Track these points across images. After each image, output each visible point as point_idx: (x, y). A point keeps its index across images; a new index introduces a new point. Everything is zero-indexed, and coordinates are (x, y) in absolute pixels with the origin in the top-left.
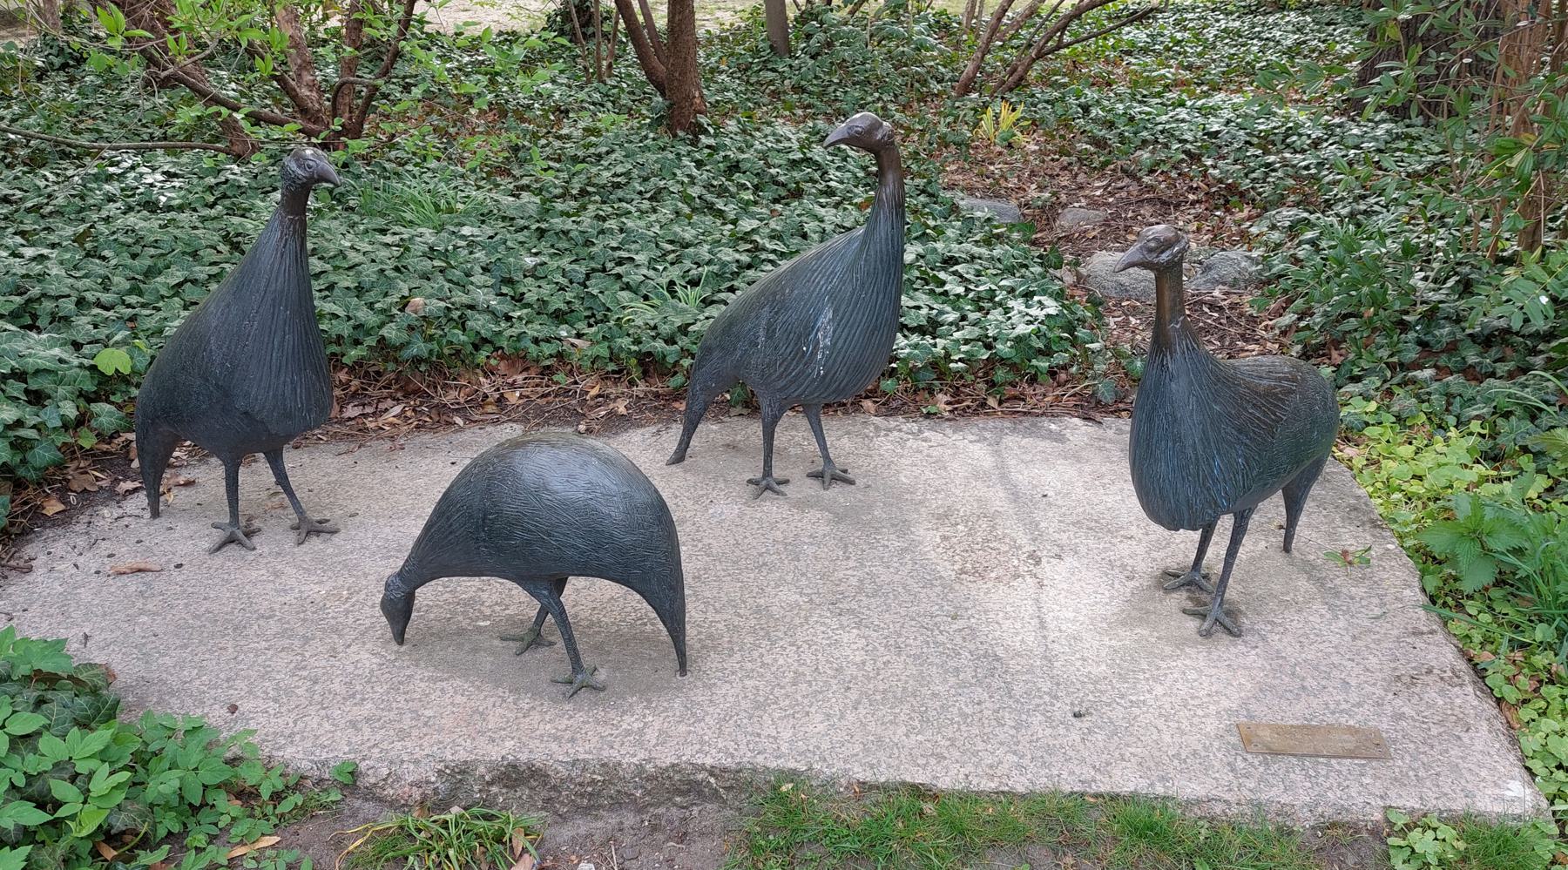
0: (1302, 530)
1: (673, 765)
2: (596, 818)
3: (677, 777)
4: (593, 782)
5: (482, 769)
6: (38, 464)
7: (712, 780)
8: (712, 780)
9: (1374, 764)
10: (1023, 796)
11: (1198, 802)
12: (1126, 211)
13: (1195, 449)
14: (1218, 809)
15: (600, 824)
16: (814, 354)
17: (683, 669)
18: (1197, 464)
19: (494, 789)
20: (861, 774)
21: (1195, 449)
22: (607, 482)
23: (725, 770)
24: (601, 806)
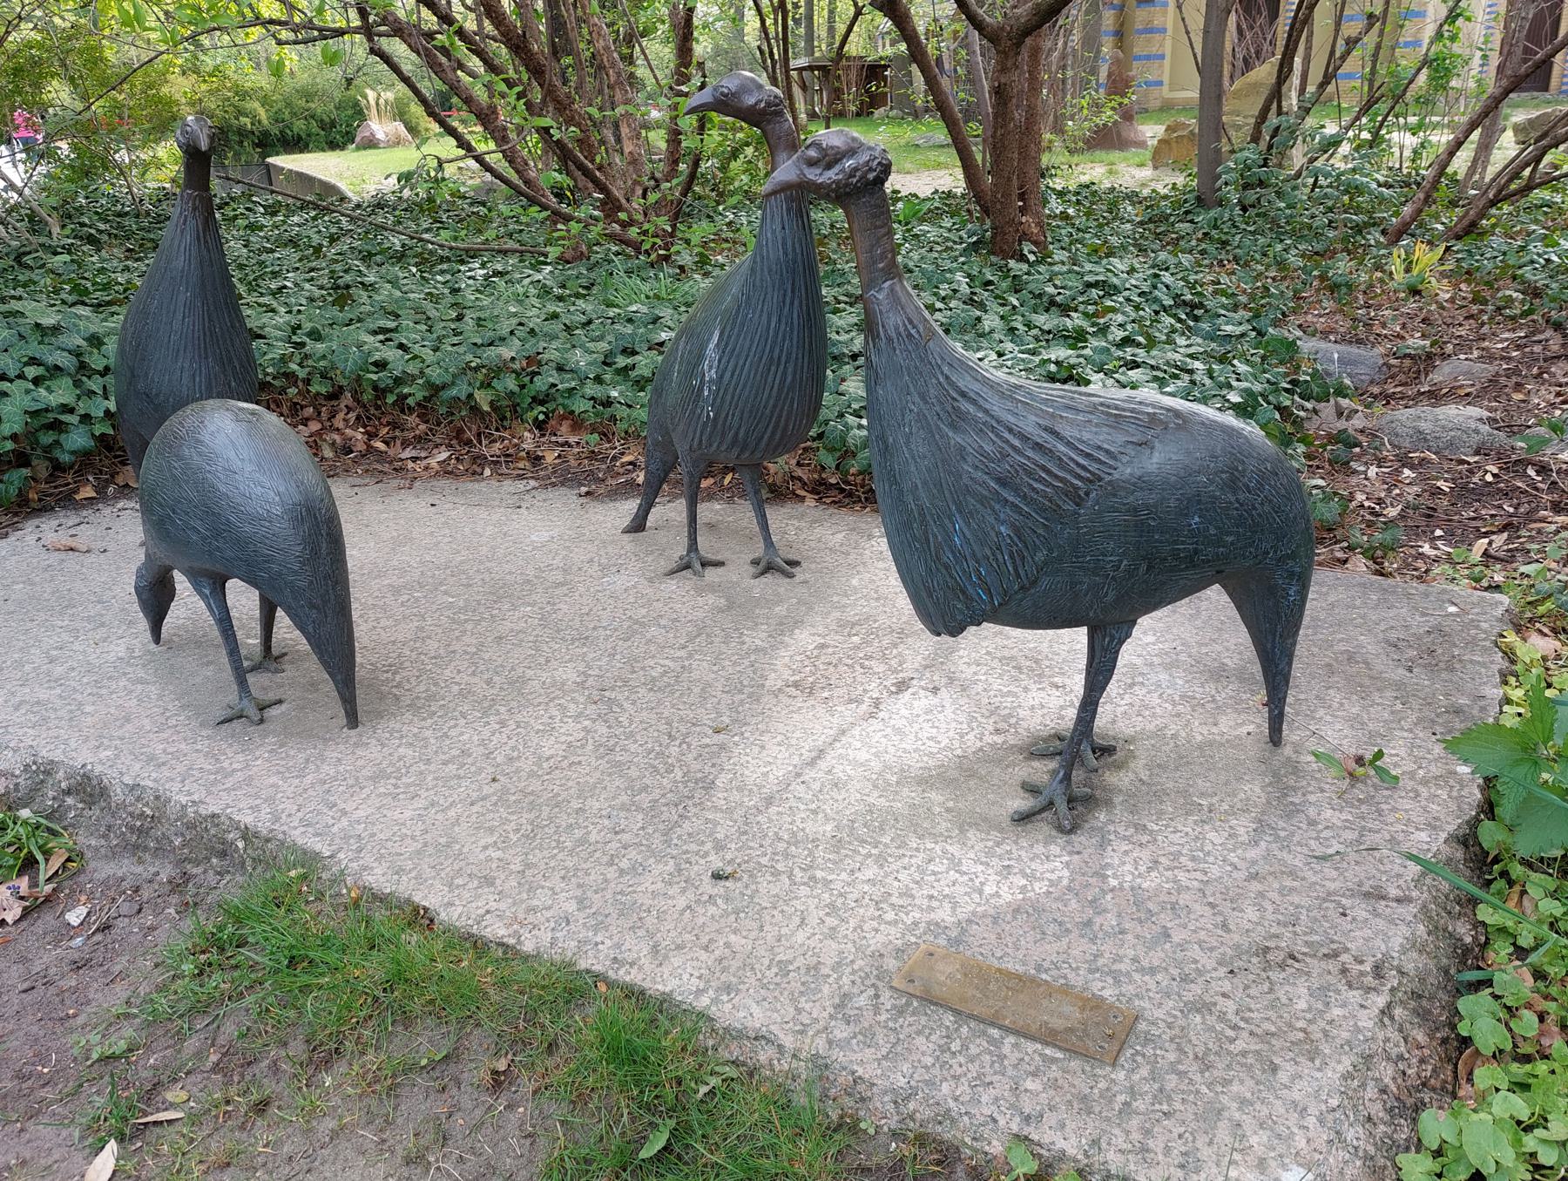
0: (65, 354)
1: (214, 816)
2: (140, 861)
3: (213, 832)
4: (142, 815)
5: (61, 775)
6: (74, 447)
7: (241, 844)
8: (241, 844)
9: (1075, 1064)
10: (526, 958)
11: (741, 1035)
12: (1529, 367)
13: (916, 499)
14: (764, 1055)
15: (139, 869)
16: (701, 389)
17: (353, 720)
18: (923, 521)
19: (70, 801)
20: (379, 879)
21: (916, 499)
22: (232, 455)
23: (256, 835)
24: (146, 849)
